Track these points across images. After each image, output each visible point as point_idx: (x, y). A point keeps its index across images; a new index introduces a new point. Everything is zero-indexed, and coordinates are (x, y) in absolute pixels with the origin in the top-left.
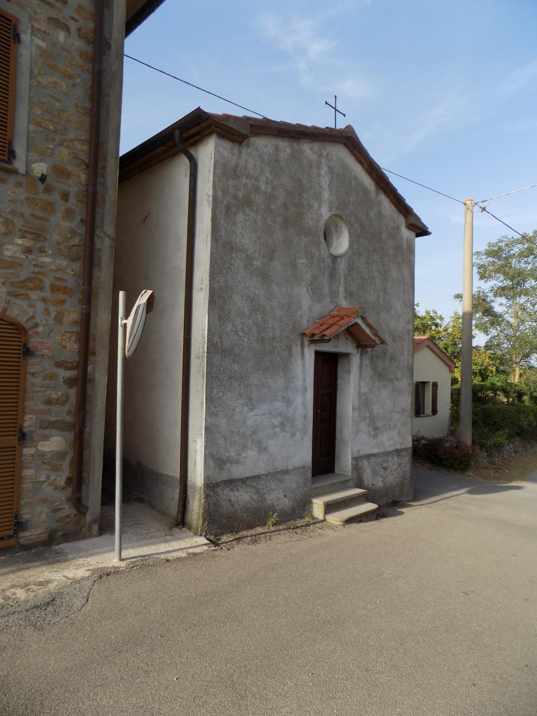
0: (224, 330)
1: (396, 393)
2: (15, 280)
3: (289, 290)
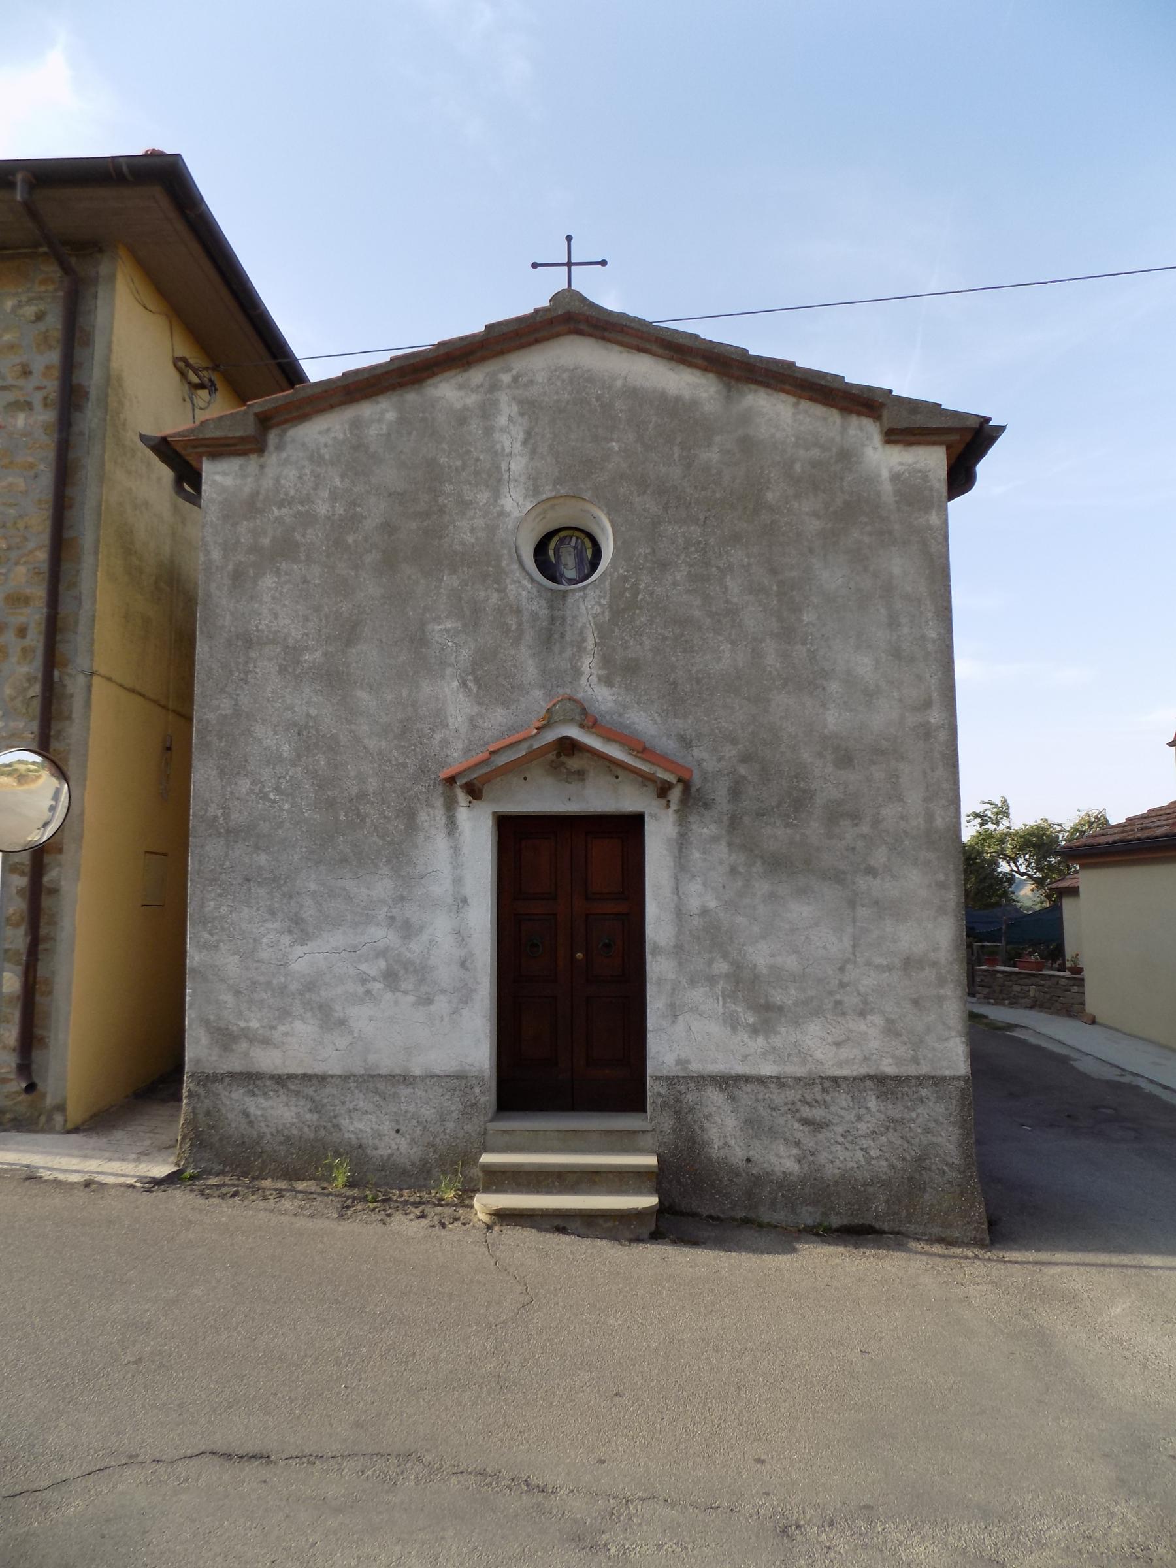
0: (232, 793)
1: (862, 912)
3: (405, 692)
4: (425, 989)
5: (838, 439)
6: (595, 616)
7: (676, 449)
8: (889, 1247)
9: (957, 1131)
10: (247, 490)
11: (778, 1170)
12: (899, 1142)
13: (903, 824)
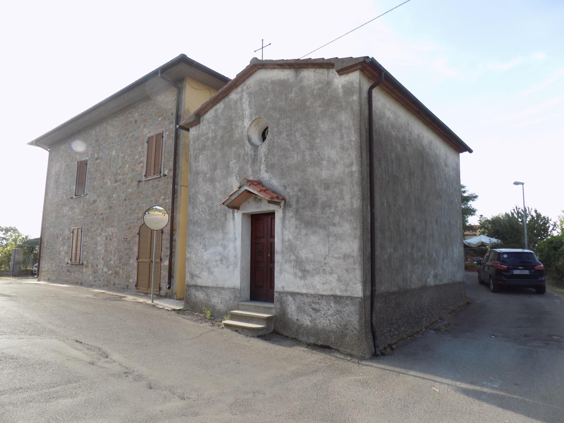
1: (331, 239)
7: (283, 96)
9: (358, 317)
12: (340, 319)
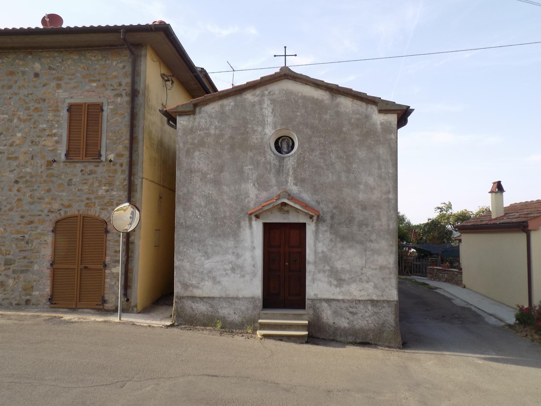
1: (368, 253)
2: (102, 203)
3: (237, 187)
4: (243, 273)
5: (365, 112)
6: (292, 165)
7: (317, 115)
8: (372, 348)
9: (394, 316)
10: (190, 126)
11: (342, 326)
13: (381, 227)
